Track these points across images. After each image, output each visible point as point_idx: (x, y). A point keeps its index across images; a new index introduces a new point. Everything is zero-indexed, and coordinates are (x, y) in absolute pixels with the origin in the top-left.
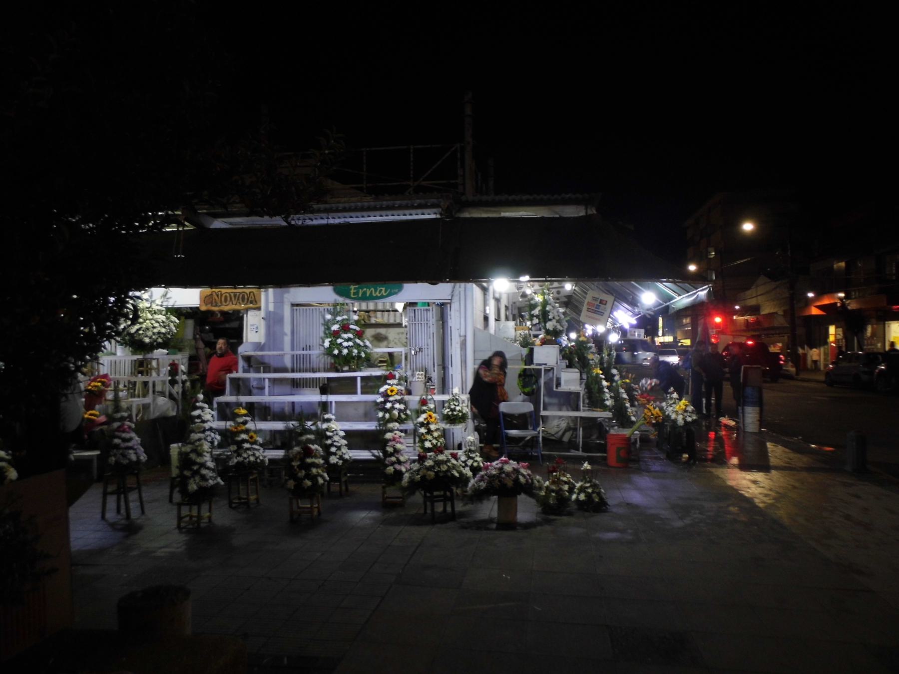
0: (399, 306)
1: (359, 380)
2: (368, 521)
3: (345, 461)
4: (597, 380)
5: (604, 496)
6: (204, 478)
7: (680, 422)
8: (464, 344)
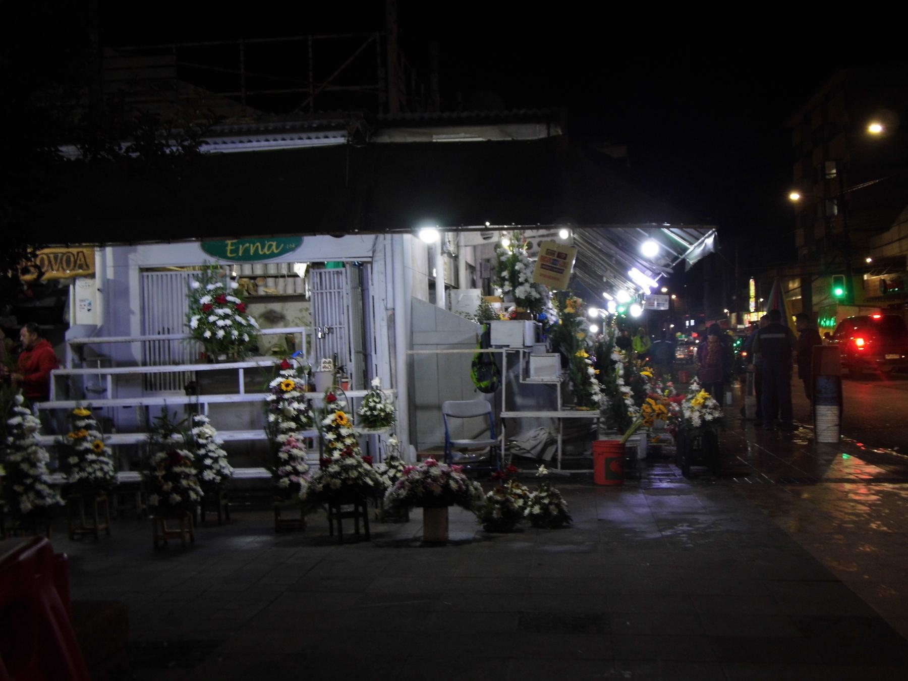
0: (300, 269)
1: (241, 372)
2: (256, 545)
3: (225, 477)
4: (582, 367)
5: (566, 509)
6: (39, 495)
7: (696, 421)
8: (391, 321)
